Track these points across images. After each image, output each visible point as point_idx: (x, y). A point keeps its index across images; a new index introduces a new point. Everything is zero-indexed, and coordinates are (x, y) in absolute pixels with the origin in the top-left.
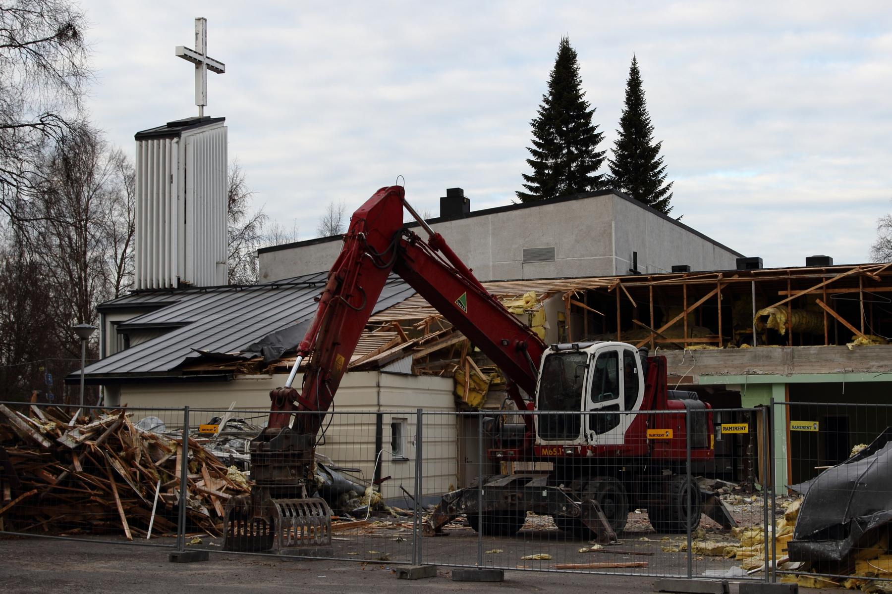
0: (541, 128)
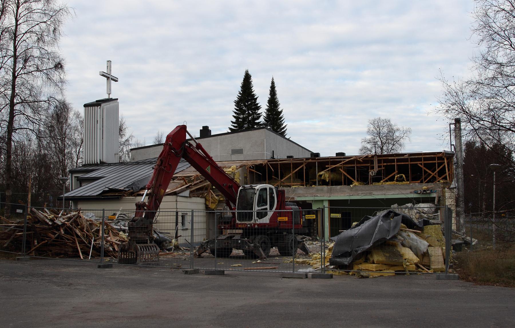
0: (238, 103)
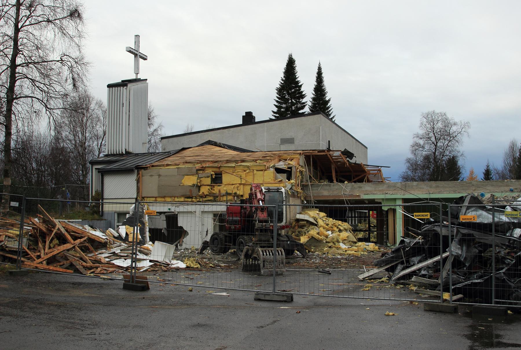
0: (280, 91)
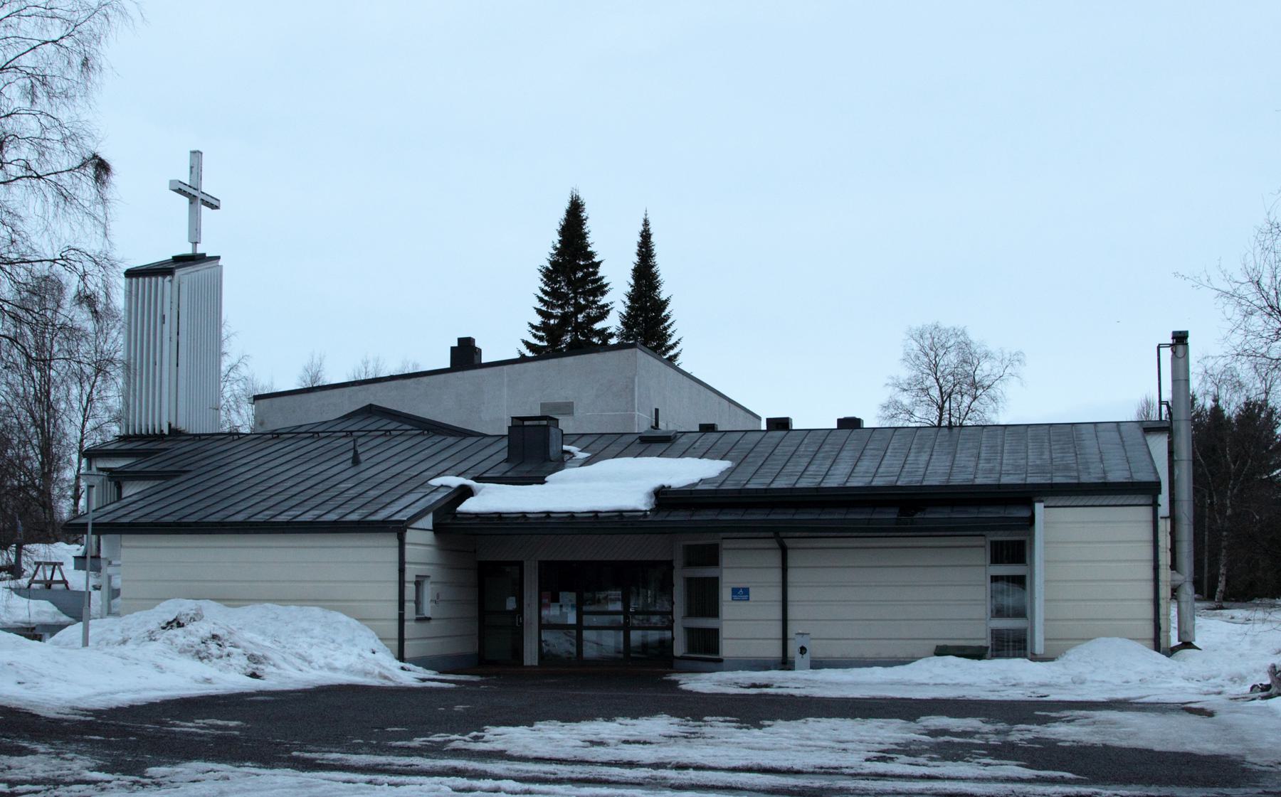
0: (550, 275)
